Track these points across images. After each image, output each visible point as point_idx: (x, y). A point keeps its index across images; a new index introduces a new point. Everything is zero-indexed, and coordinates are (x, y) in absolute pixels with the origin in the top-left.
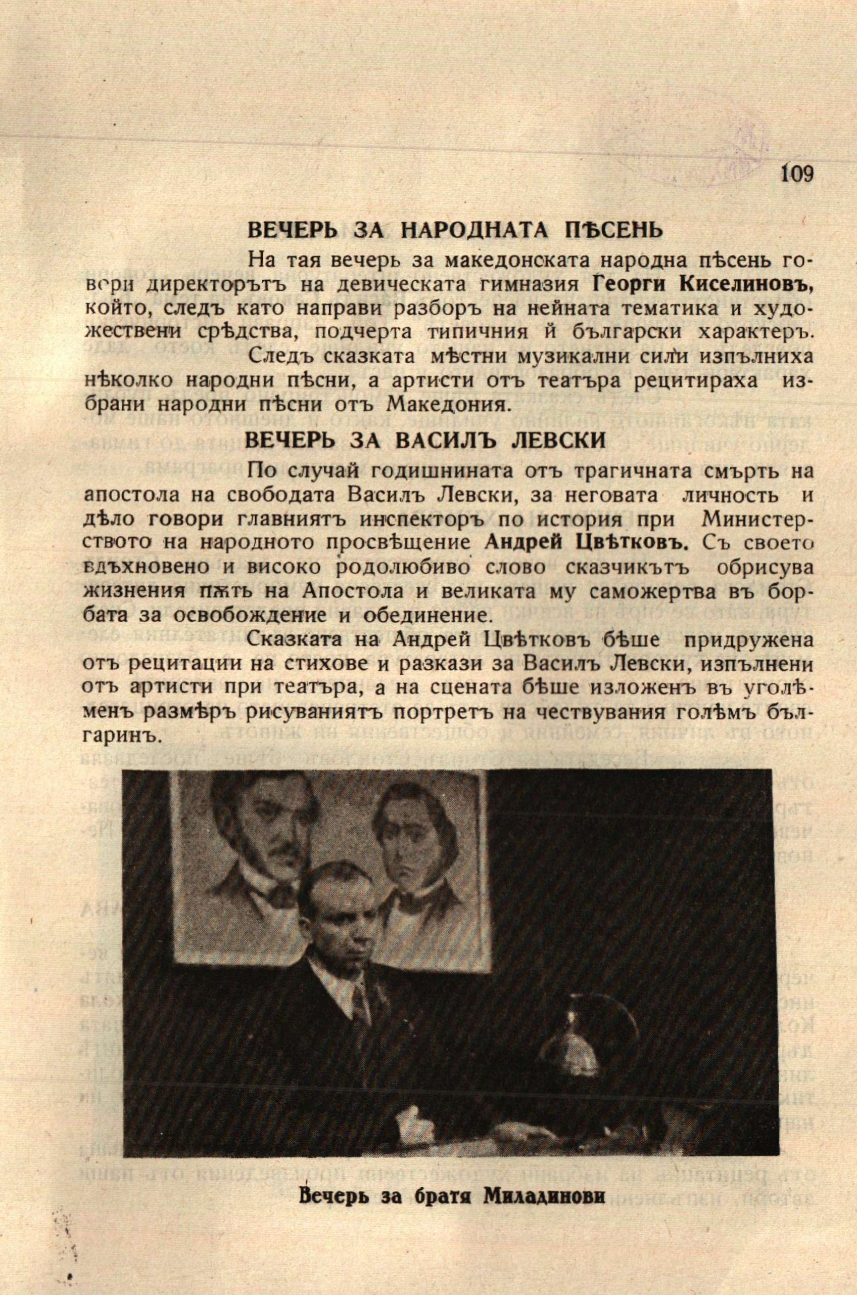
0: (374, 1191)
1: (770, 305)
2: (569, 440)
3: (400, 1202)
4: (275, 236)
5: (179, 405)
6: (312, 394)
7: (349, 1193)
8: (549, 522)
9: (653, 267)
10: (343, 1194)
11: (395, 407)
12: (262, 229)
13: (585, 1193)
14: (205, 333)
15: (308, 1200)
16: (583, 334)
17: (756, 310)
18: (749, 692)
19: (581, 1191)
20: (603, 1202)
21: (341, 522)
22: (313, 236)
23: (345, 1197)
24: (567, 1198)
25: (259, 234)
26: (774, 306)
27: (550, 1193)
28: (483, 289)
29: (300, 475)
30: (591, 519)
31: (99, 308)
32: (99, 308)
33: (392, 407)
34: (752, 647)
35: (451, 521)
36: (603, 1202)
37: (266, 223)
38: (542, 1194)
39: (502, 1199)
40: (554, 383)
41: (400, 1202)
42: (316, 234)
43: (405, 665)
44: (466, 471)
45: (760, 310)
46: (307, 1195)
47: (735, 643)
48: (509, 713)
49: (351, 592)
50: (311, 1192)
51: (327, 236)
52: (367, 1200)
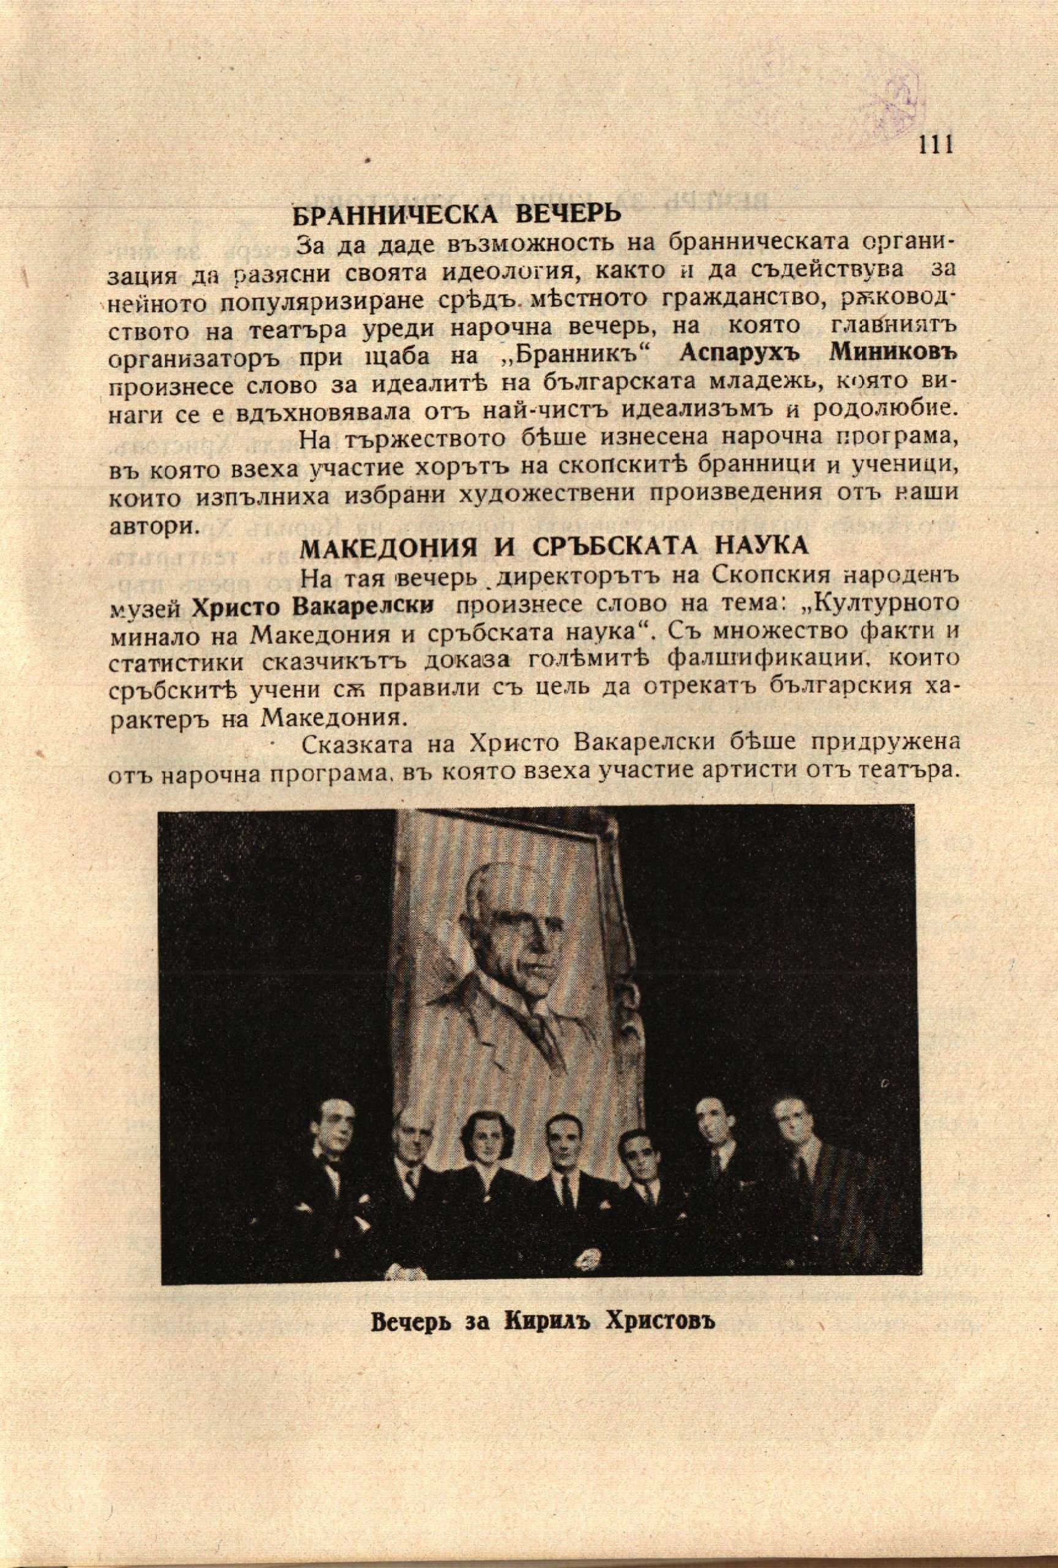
1: (477, 491)
2: (620, 545)
4: (548, 221)
5: (611, 382)
7: (428, 1319)
9: (937, 303)
10: (421, 1320)
11: (261, 638)
12: (533, 213)
13: (691, 1317)
15: (382, 1329)
17: (462, 495)
18: (369, 335)
19: (687, 1315)
22: (591, 219)
23: (424, 1324)
25: (530, 218)
26: (482, 492)
29: (261, 391)
31: (905, 658)
32: (905, 658)
33: (257, 639)
37: (538, 206)
39: (522, 1325)
42: (596, 217)
43: (821, 409)
44: (792, 492)
46: (381, 1323)
47: (871, 746)
50: (386, 1319)
51: (608, 219)
52: (449, 1326)
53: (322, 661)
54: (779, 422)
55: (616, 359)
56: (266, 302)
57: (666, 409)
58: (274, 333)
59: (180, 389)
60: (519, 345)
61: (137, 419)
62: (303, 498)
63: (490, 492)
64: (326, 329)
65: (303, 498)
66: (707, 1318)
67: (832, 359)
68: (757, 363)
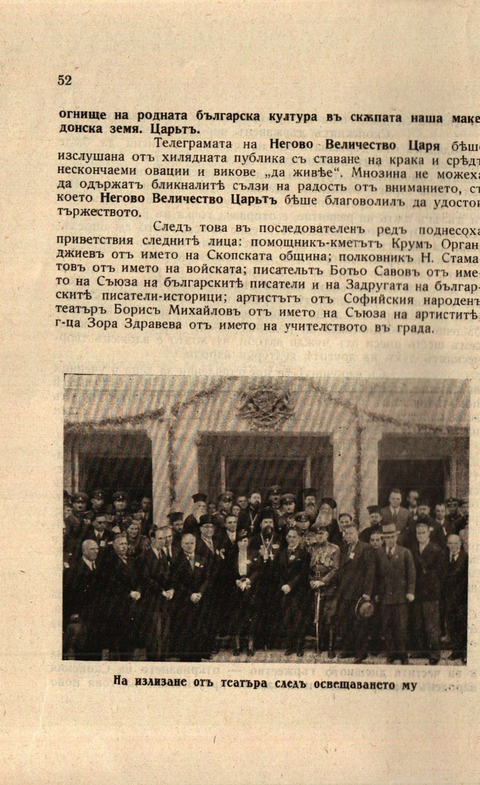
0: (399, 683)
3: (126, 684)
6: (311, 195)
7: (341, 683)
8: (171, 298)
10: (338, 683)
14: (451, 162)
16: (255, 312)
20: (137, 679)
21: (157, 312)
24: (378, 118)
27: (156, 679)
28: (60, 214)
30: (195, 297)
34: (377, 289)
35: (188, 297)
36: (137, 679)
38: (151, 680)
40: (316, 328)
41: (126, 684)
45: (166, 158)
46: (117, 679)
47: (140, 325)
48: (266, 327)
49: (460, 204)
53: (103, 170)
54: (193, 178)
55: (403, 261)
56: (242, 158)
57: (69, 309)
58: (142, 297)
59: (206, 186)
60: (116, 305)
61: (346, 202)
62: (169, 158)
63: (441, 202)
64: (76, 211)
65: (169, 158)
66: (302, 683)
67: (170, 313)
68: (409, 250)
